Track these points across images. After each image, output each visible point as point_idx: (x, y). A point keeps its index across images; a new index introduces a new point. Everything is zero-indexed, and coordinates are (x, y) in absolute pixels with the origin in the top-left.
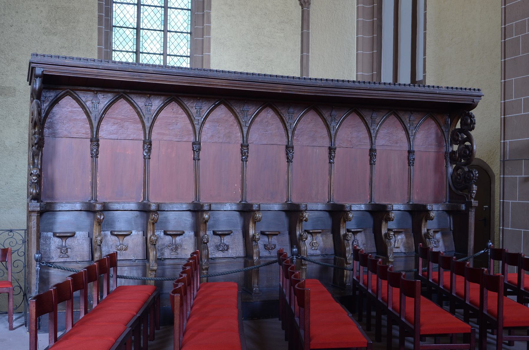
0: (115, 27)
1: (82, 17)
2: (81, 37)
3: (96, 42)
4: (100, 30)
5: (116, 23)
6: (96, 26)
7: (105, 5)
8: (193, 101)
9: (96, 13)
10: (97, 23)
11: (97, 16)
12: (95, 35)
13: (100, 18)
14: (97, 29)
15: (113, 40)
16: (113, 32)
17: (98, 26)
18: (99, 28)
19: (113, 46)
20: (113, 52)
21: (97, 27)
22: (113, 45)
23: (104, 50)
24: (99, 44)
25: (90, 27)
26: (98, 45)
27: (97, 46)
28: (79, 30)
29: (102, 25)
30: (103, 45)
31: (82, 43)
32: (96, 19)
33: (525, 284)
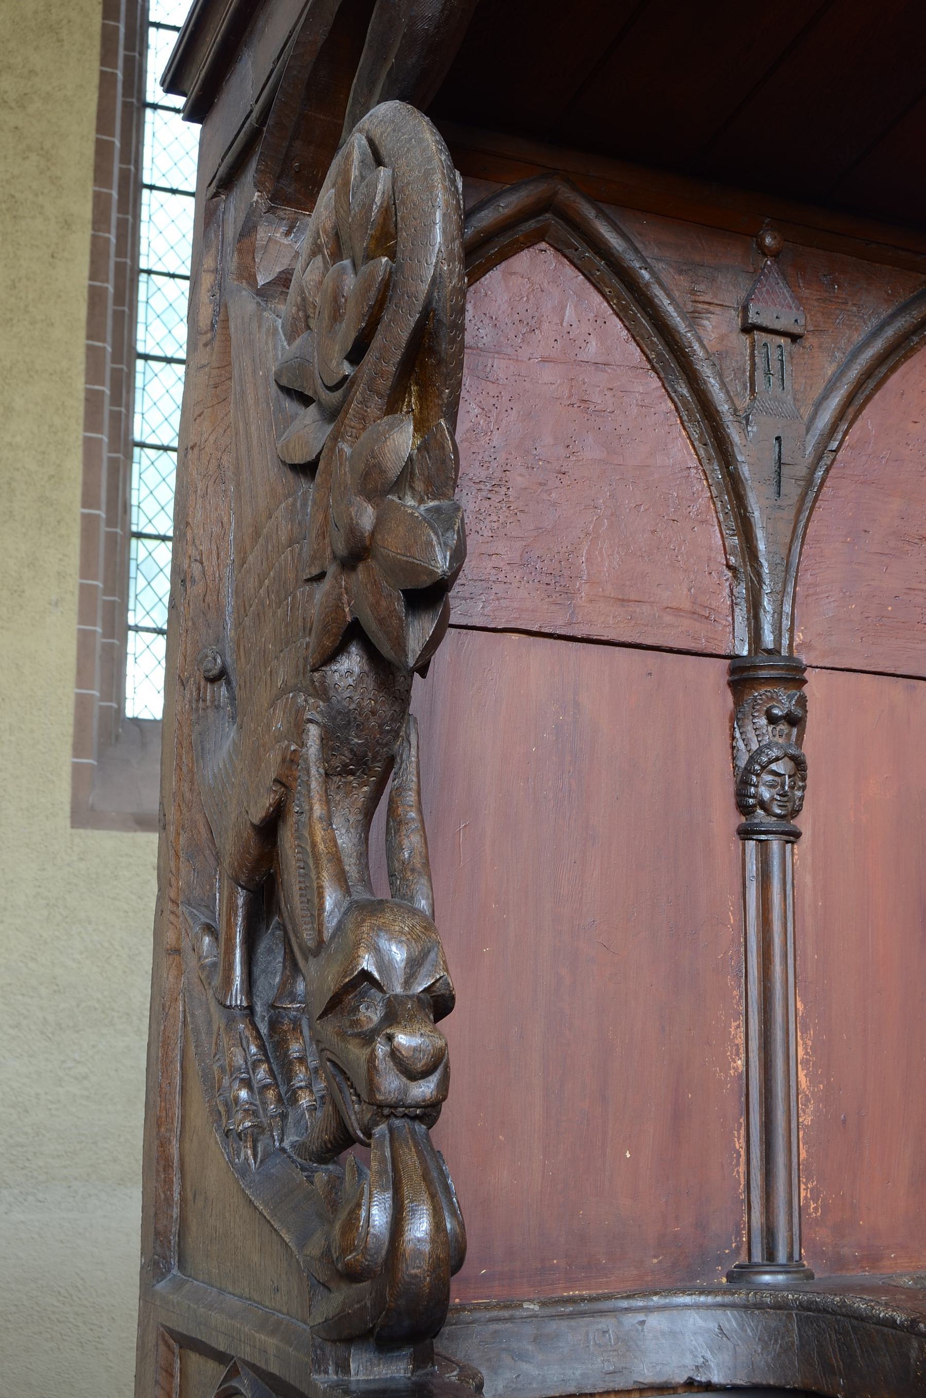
0: (142, 445)
1: (23, 395)
2: (18, 470)
3: (74, 493)
4: (90, 448)
5: (147, 430)
6: (76, 433)
7: (104, 635)
8: (337, 1270)
9: (80, 384)
10: (81, 421)
11: (82, 395)
12: (74, 465)
13: (92, 400)
14: (80, 442)
15: (134, 494)
16: (135, 467)
17: (86, 430)
18: (87, 441)
19: (134, 520)
20: (134, 541)
21: (81, 437)
22: (132, 670)
23: (100, 641)
24: (88, 500)
25: (55, 433)
26: (85, 504)
27: (78, 510)
28: (11, 444)
29: (98, 430)
30: (103, 506)
31: (22, 494)
32: (78, 407)
33: (653, 374)
